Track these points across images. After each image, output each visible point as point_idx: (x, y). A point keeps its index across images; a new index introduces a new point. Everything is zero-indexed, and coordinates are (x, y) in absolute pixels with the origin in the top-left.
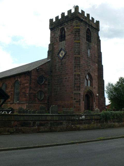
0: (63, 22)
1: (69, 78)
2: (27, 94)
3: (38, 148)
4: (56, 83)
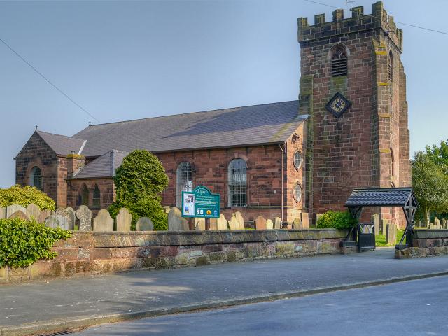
1: (359, 158)
2: (275, 189)
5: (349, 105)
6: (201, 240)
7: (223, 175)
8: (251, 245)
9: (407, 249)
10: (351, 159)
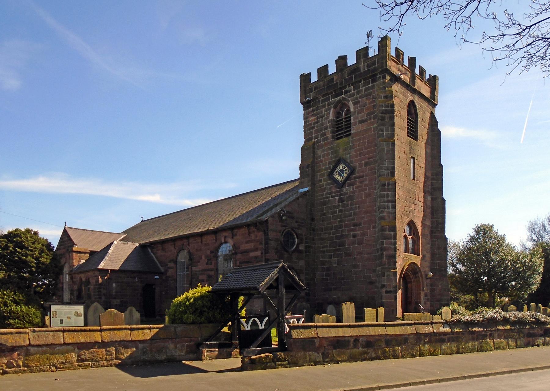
0: (342, 84)
3: (541, 369)
4: (326, 247)
5: (352, 172)
7: (213, 262)
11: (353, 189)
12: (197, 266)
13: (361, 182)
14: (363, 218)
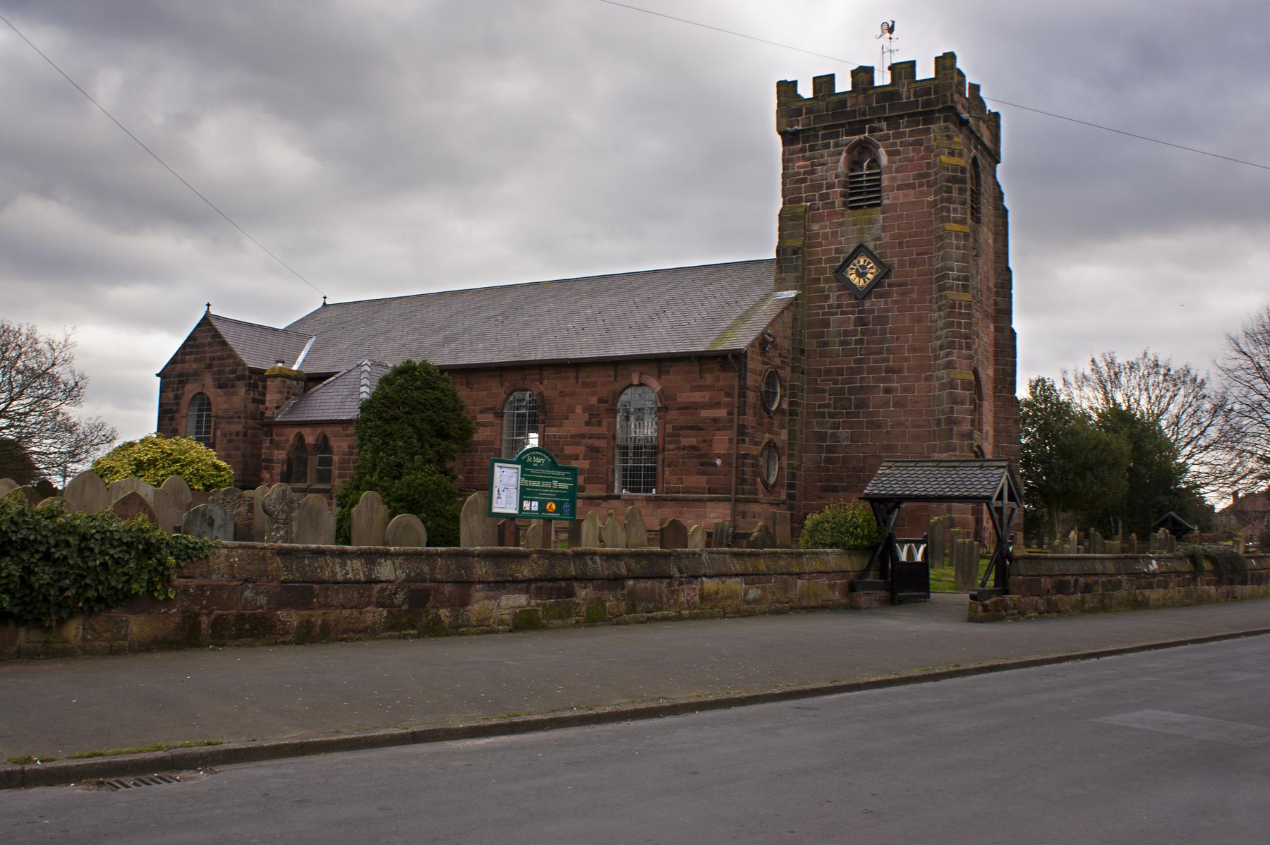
1: (905, 390)
2: (719, 456)
4: (828, 406)
6: (525, 571)
7: (605, 423)
8: (642, 584)
9: (995, 599)
10: (887, 391)
11: (886, 303)
12: (560, 426)
13: (903, 294)
14: (907, 359)
